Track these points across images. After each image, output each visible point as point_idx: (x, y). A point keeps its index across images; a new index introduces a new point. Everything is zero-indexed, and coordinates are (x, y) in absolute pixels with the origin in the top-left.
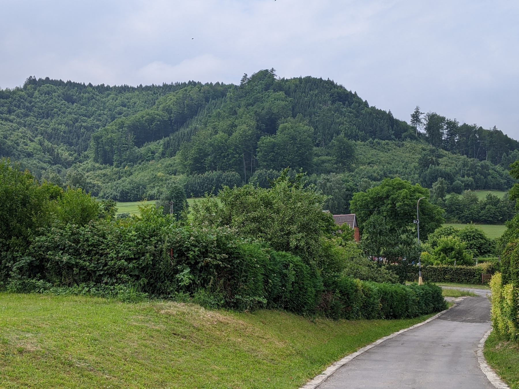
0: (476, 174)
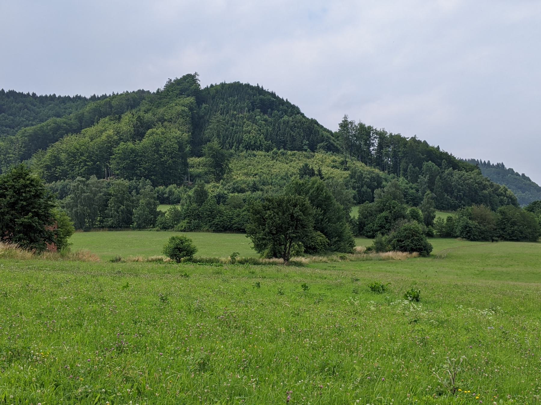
0: (362, 186)
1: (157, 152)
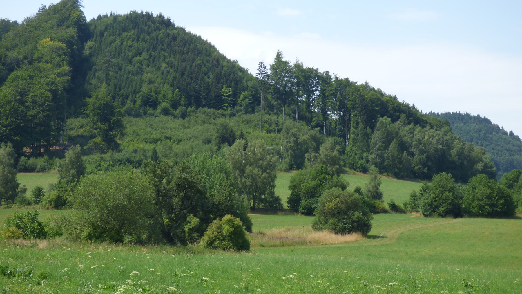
1: (22, 102)
